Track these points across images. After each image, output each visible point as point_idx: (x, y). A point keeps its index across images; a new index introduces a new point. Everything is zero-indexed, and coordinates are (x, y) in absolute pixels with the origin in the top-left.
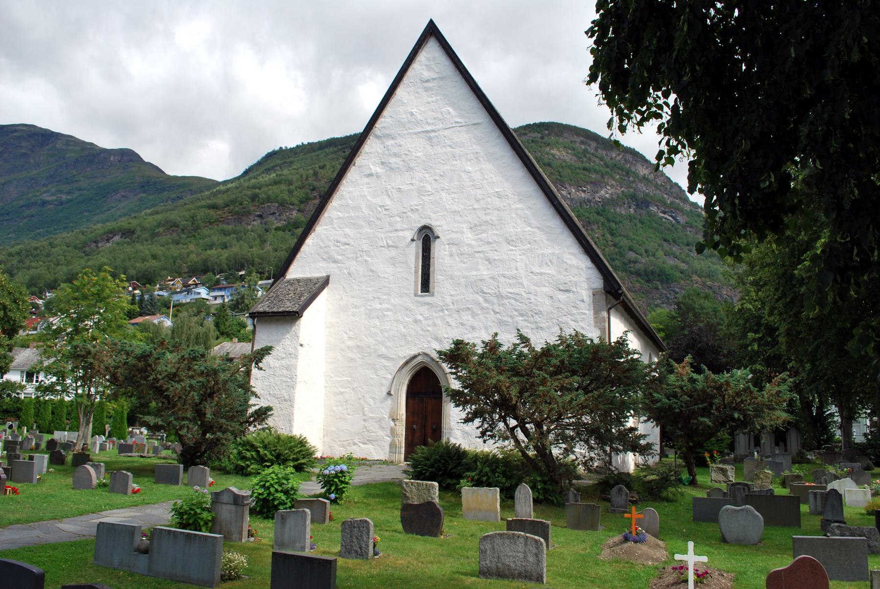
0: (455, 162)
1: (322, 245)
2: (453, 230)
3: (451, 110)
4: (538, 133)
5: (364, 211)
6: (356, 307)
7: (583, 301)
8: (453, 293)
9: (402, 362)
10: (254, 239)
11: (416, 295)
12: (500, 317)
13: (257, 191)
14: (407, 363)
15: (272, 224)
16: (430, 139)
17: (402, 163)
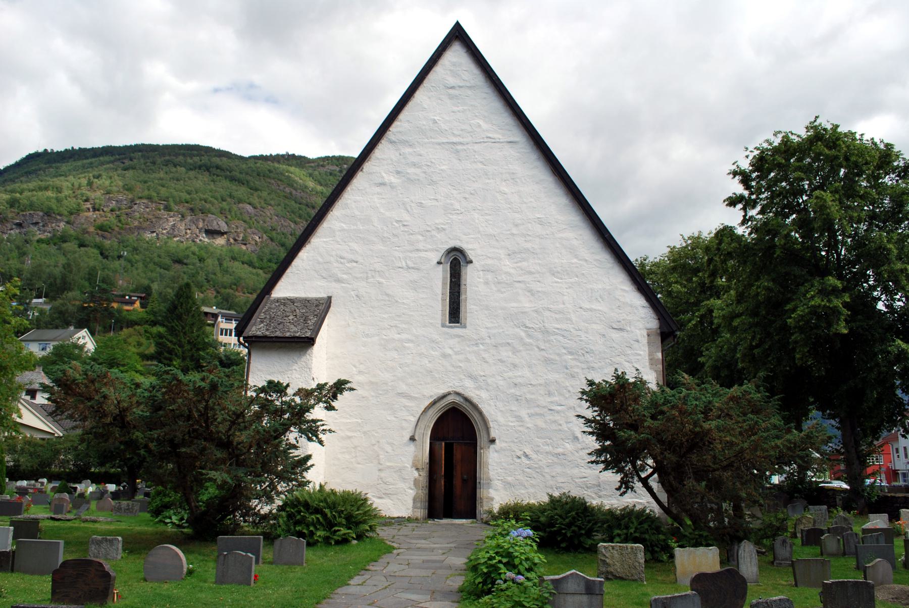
0: (487, 181)
1: (320, 260)
2: (489, 255)
3: (481, 123)
4: (337, 166)
5: (376, 224)
6: (367, 336)
7: (638, 341)
8: (489, 325)
9: (427, 403)
10: (11, 251)
11: (443, 326)
12: (546, 355)
13: (18, 195)
14: (434, 403)
15: (34, 235)
16: (457, 151)
17: (424, 175)
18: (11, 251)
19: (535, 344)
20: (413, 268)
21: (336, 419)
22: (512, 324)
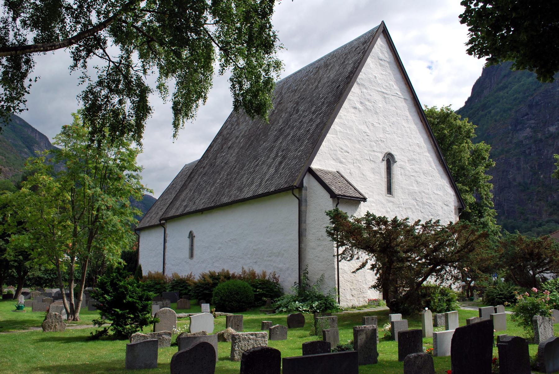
16: (385, 98)
20: (372, 161)
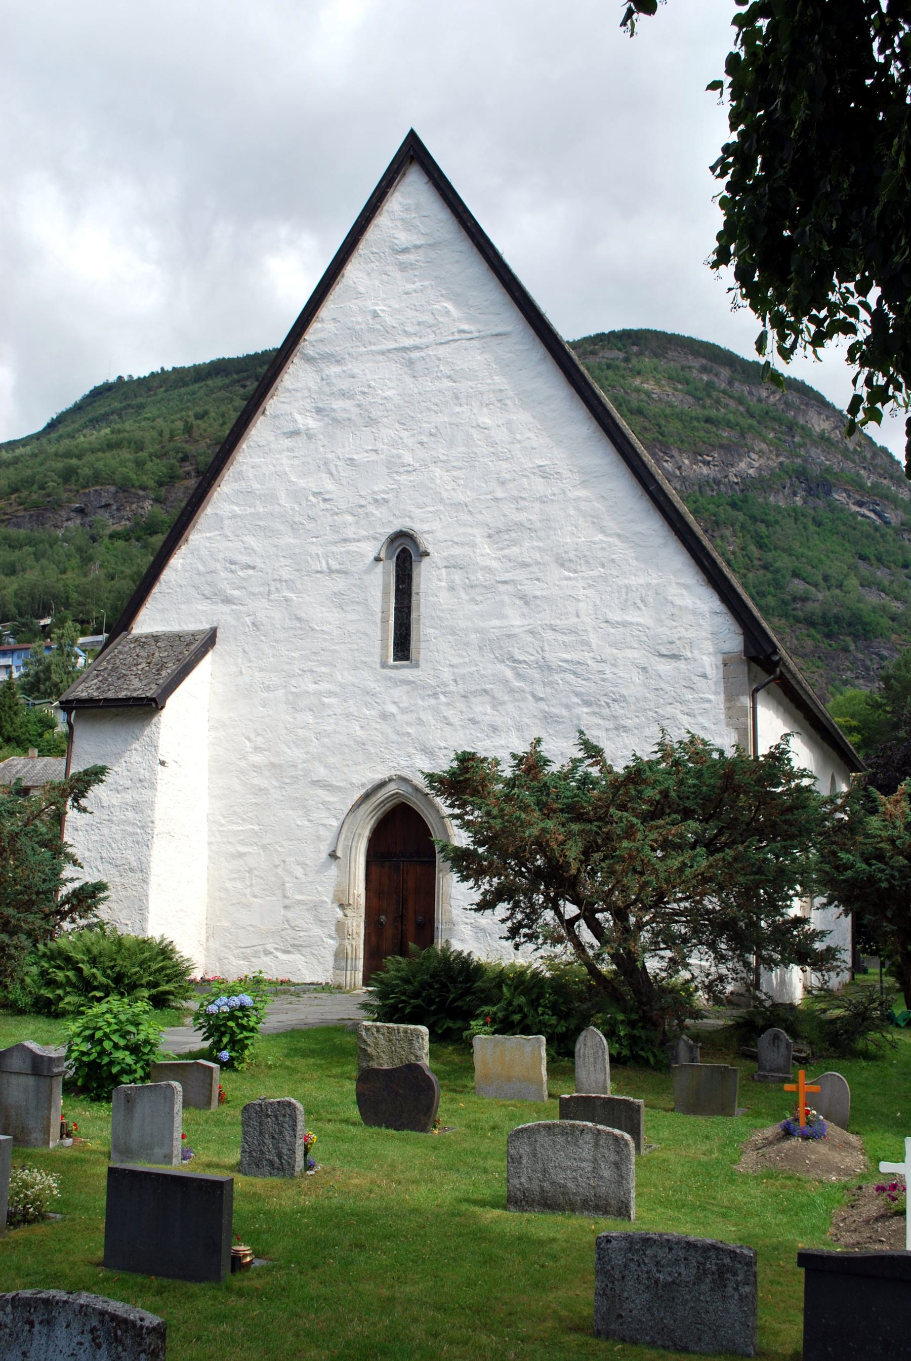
0: (458, 409)
1: (201, 568)
3: (450, 306)
4: (619, 350)
5: (282, 502)
6: (268, 689)
7: (704, 676)
8: (456, 661)
10: (69, 556)
11: (384, 665)
13: (74, 461)
14: (367, 796)
15: (104, 526)
16: (411, 363)
17: (357, 410)
18: (69, 556)
19: (527, 689)
20: (338, 572)
21: (222, 825)
22: (492, 656)
